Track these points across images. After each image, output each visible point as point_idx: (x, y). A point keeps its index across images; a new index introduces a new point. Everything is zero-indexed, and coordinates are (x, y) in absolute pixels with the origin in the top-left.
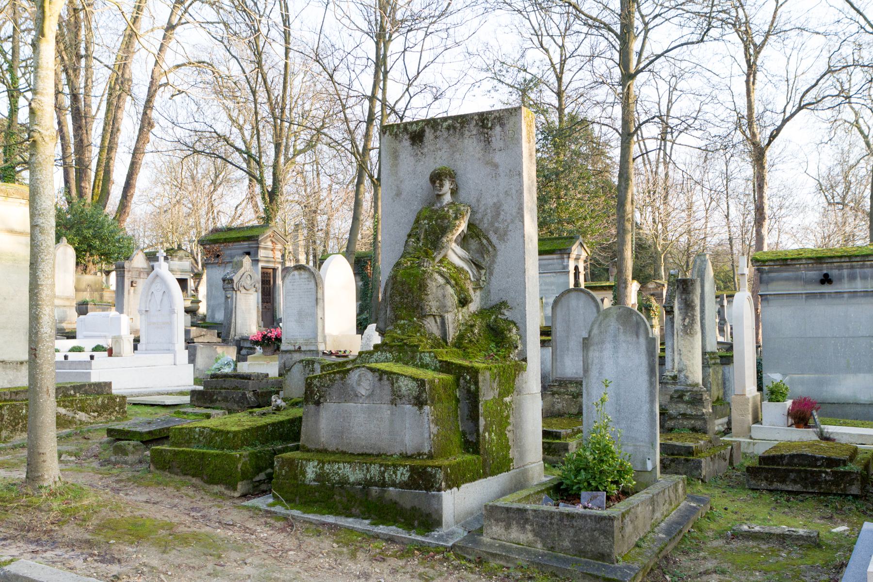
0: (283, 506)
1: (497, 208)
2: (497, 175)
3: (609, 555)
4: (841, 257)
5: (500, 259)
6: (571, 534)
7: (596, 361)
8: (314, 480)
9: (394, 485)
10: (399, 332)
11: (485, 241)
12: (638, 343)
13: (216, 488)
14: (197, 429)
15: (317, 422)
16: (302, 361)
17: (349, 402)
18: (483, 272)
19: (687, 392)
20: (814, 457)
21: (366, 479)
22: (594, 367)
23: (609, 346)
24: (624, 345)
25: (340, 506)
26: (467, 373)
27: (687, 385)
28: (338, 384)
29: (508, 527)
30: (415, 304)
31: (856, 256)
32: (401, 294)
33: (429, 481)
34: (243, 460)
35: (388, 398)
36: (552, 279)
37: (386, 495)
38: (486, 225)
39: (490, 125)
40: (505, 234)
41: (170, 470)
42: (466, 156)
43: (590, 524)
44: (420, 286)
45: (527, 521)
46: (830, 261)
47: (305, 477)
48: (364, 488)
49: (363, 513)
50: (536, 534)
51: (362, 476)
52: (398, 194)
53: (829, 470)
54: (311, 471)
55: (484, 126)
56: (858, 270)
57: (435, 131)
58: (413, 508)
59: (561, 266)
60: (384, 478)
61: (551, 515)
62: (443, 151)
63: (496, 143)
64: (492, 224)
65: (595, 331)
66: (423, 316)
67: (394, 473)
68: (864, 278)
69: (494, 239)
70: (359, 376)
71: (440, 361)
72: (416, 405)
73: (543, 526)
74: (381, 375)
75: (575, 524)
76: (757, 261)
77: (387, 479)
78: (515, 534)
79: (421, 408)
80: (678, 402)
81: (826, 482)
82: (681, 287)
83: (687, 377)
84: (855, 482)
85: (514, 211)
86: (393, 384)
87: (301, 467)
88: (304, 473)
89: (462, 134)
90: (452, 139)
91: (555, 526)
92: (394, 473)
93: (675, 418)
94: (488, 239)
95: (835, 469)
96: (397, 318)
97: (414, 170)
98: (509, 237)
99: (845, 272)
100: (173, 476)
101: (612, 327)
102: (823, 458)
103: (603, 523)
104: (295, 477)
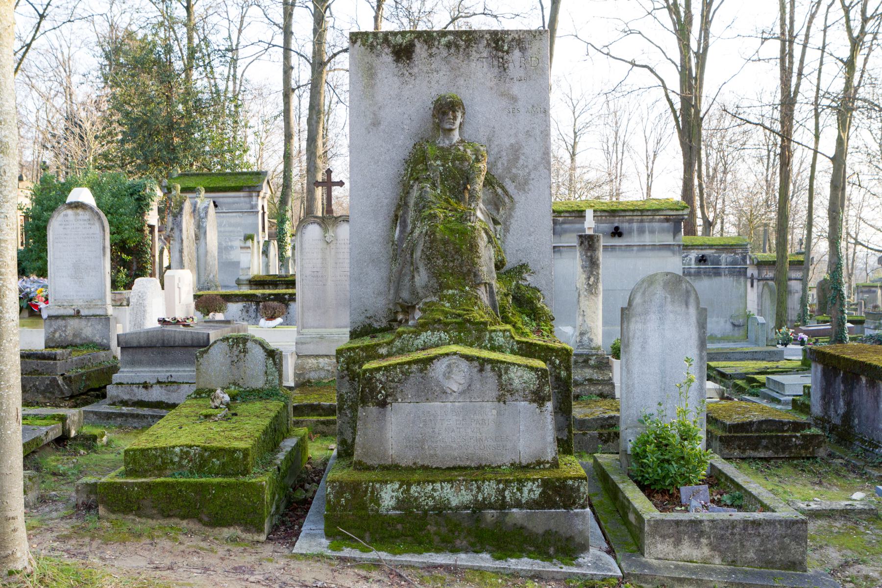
1: (516, 151)
2: (514, 111)
3: (801, 563)
4: (633, 211)
5: (518, 213)
6: (757, 544)
7: (638, 334)
9: (519, 505)
10: (448, 305)
11: (499, 191)
12: (687, 314)
13: (227, 532)
14: (177, 450)
15: (382, 429)
16: (227, 339)
17: (433, 401)
18: (498, 227)
19: (593, 355)
20: (782, 422)
21: (476, 500)
22: (636, 340)
23: (653, 317)
24: (671, 315)
25: (437, 539)
26: (556, 357)
27: (591, 349)
29: (678, 543)
30: (465, 269)
31: (648, 210)
32: (444, 256)
33: (570, 496)
36: (238, 220)
38: (500, 171)
39: (506, 48)
40: (526, 182)
41: (139, 512)
42: (473, 80)
43: (780, 530)
44: (471, 245)
45: (702, 534)
46: (623, 214)
47: (379, 505)
48: (474, 512)
50: (714, 548)
51: (470, 497)
52: (376, 123)
53: (798, 434)
54: (388, 496)
55: (498, 48)
56: (646, 224)
57: (430, 47)
58: (548, 533)
59: (249, 206)
60: (504, 497)
61: (733, 524)
62: (441, 73)
63: (515, 70)
64: (508, 169)
65: (638, 300)
66: (476, 285)
68: (652, 232)
69: (511, 187)
70: (449, 366)
72: (534, 401)
73: (722, 537)
75: (762, 531)
77: (508, 499)
78: (687, 550)
80: (583, 367)
81: (796, 446)
82: (586, 243)
83: (591, 340)
84: (823, 445)
85: (538, 156)
86: (500, 376)
87: (372, 492)
88: (377, 500)
89: (468, 56)
90: (453, 59)
91: (737, 537)
93: (582, 384)
94: (503, 188)
95: (803, 432)
96: (442, 287)
97: (408, 97)
98: (531, 187)
99: (635, 225)
100: (143, 520)
101: (658, 296)
102: (789, 422)
103: (795, 528)
104: (364, 507)
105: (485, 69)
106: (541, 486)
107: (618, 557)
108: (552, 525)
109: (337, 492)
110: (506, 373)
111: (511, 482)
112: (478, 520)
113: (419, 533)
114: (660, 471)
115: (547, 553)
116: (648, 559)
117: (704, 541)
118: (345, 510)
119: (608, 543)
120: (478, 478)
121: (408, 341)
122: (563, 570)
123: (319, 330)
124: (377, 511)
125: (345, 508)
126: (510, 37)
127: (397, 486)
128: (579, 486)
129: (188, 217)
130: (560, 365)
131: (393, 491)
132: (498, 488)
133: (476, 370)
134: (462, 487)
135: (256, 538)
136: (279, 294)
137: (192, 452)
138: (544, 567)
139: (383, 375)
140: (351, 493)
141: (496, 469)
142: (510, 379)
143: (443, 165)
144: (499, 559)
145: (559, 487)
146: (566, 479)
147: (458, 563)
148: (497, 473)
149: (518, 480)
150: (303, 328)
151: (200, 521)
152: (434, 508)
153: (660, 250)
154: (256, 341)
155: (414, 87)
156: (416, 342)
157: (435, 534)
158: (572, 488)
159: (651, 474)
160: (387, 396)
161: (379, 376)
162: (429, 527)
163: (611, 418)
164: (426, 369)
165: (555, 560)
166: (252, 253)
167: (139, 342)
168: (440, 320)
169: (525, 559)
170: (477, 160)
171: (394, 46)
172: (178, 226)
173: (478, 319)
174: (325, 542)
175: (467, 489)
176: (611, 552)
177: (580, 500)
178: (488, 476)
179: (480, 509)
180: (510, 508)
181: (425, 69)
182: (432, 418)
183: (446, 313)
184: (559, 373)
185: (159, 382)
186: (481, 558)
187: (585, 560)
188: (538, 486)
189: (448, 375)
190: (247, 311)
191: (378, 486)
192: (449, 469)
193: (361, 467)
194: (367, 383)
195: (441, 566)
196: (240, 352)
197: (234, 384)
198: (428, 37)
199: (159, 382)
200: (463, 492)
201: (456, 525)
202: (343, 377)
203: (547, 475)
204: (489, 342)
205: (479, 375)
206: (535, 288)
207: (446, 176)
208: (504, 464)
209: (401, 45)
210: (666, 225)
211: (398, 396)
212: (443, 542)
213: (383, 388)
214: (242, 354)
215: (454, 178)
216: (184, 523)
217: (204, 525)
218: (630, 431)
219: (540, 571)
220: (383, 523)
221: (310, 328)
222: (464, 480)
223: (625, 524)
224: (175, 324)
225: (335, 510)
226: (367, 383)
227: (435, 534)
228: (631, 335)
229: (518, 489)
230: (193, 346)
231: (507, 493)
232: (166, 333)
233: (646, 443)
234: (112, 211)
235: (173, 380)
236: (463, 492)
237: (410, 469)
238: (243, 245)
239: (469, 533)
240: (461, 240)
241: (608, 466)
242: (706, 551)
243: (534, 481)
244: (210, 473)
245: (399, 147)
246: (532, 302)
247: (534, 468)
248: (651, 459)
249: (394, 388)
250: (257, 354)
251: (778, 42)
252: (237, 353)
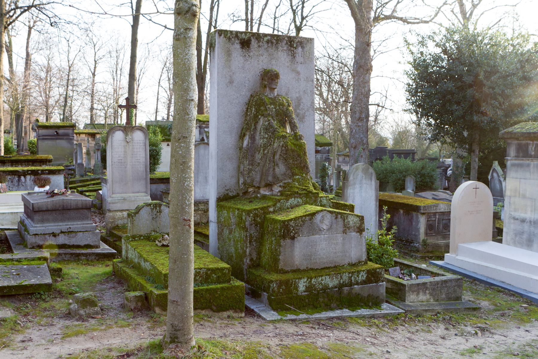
1: (299, 101)
2: (298, 80)
7: (351, 195)
8: (304, 292)
9: (357, 284)
13: (225, 314)
16: (150, 205)
17: (315, 235)
21: (340, 283)
23: (357, 186)
25: (323, 305)
29: (418, 294)
30: (302, 165)
35: (341, 229)
37: (353, 291)
39: (295, 46)
40: (304, 117)
45: (427, 288)
47: (298, 291)
48: (339, 289)
49: (338, 306)
50: (431, 294)
51: (337, 282)
52: (231, 82)
54: (302, 285)
55: (291, 46)
57: (259, 42)
58: (369, 295)
60: (351, 280)
62: (264, 57)
63: (299, 59)
67: (358, 276)
70: (323, 217)
72: (358, 232)
74: (337, 215)
76: (200, 121)
77: (353, 281)
79: (361, 234)
85: (309, 103)
86: (344, 220)
87: (295, 284)
88: (297, 288)
89: (277, 48)
90: (270, 49)
96: (294, 174)
97: (247, 68)
98: (305, 120)
104: (290, 292)
105: (285, 56)
115: (369, 306)
116: (407, 303)
117: (427, 292)
123: (123, 195)
126: (297, 40)
135: (240, 315)
136: (34, 170)
137: (202, 271)
143: (275, 108)
150: (113, 194)
151: (212, 310)
152: (322, 289)
155: (251, 63)
156: (287, 204)
157: (322, 302)
161: (292, 223)
167: (47, 207)
170: (289, 106)
171: (241, 40)
175: (336, 278)
179: (341, 287)
181: (256, 54)
185: (62, 232)
189: (322, 221)
190: (12, 182)
191: (297, 281)
192: (322, 269)
196: (157, 212)
197: (154, 231)
198: (258, 36)
199: (62, 232)
202: (252, 225)
207: (278, 114)
208: (345, 264)
209: (244, 39)
211: (300, 233)
214: (159, 214)
215: (281, 115)
216: (203, 312)
217: (214, 311)
221: (117, 193)
224: (61, 195)
227: (322, 302)
230: (82, 209)
232: (65, 201)
235: (71, 230)
240: (299, 150)
242: (428, 296)
243: (363, 271)
244: (212, 283)
245: (244, 95)
251: (244, 22)
252: (155, 213)
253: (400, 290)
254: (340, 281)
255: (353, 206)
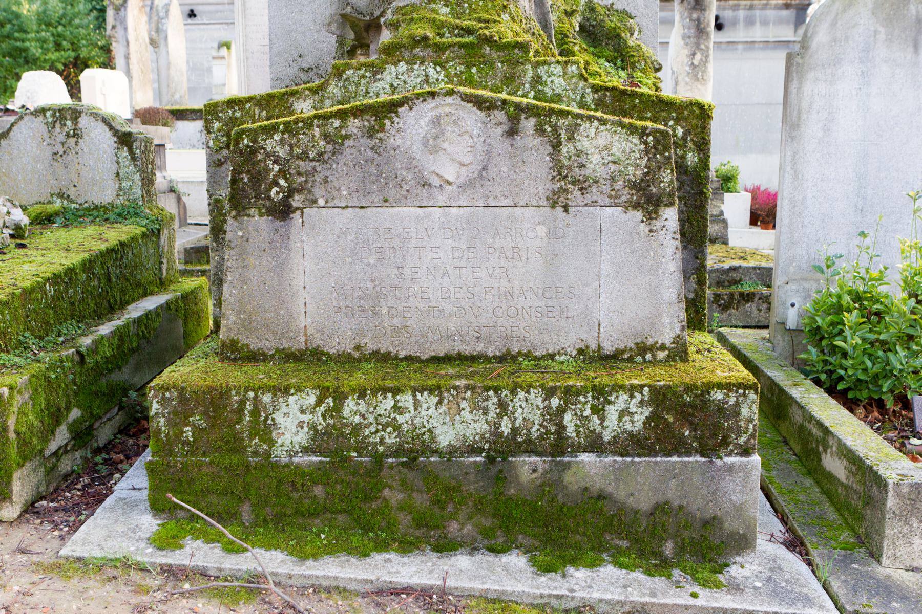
0: (211, 538)
8: (306, 450)
9: (595, 445)
10: (445, 10)
15: (280, 268)
17: (398, 203)
21: (496, 433)
25: (404, 520)
26: (677, 120)
28: (357, 148)
33: (717, 427)
34: (18, 400)
35: (544, 187)
47: (272, 443)
48: (491, 460)
54: (293, 423)
58: (661, 508)
60: (562, 427)
67: (597, 410)
68: (765, 23)
70: (436, 122)
71: (596, 89)
72: (636, 206)
77: (570, 431)
79: (651, 215)
86: (556, 146)
87: (255, 413)
88: (265, 430)
92: (597, 410)
99: (741, 14)
104: (235, 445)
106: (650, 403)
107: (817, 560)
108: (672, 493)
109: (175, 412)
110: (570, 139)
111: (578, 393)
112: (501, 478)
113: (365, 507)
114: (869, 364)
115: (658, 555)
116: (889, 569)
118: (193, 454)
119: (784, 520)
120: (501, 383)
121: (358, 85)
122: (699, 602)
124: (267, 455)
125: (193, 448)
127: (312, 399)
128: (737, 405)
129: (136, 11)
130: (684, 139)
131: (303, 412)
132: (548, 407)
133: (500, 130)
134: (464, 404)
138: (653, 594)
139: (282, 141)
140: (205, 414)
141: (542, 362)
142: (579, 153)
144: (547, 569)
145: (692, 405)
146: (709, 387)
147: (451, 583)
148: (545, 371)
149: (594, 388)
152: (398, 451)
153: (775, 48)
154: (95, 115)
157: (401, 509)
158: (721, 408)
159: (850, 370)
160: (291, 192)
161: (271, 144)
162: (386, 492)
163: (734, 269)
164: (382, 129)
165: (676, 572)
166: (229, 66)
168: (425, 38)
169: (609, 571)
172: (121, 23)
173: (509, 37)
174: (149, 523)
175: (475, 408)
176: (795, 544)
177: (739, 435)
178: (526, 378)
180: (574, 453)
182: (396, 243)
183: (439, 27)
184: (683, 157)
186: (505, 568)
187: (746, 572)
188: (642, 403)
189: (433, 142)
191: (267, 398)
193: (234, 353)
194: (245, 163)
195: (408, 590)
196: (68, 135)
197: (61, 195)
200: (466, 414)
201: (448, 489)
202: (220, 164)
203: (663, 376)
204: (533, 87)
205: (508, 141)
206: (624, 12)
208: (563, 351)
210: (785, 13)
211: (318, 192)
212: (419, 526)
213: (282, 173)
214: (72, 141)
218: (793, 286)
219: (644, 605)
220: (280, 481)
222: (467, 388)
223: (810, 473)
225: (171, 453)
226: (245, 163)
227: (401, 509)
228: (805, 105)
229: (595, 410)
231: (568, 417)
233: (838, 309)
234: (64, 21)
236: (466, 414)
237: (349, 361)
238: (215, 54)
239: (479, 506)
241: (753, 351)
243: (632, 390)
246: (618, 36)
247: (630, 360)
248: (852, 341)
249: (307, 174)
250: (99, 140)
252: (62, 137)
253: (869, 501)
254: (497, 425)
255: (701, 106)
